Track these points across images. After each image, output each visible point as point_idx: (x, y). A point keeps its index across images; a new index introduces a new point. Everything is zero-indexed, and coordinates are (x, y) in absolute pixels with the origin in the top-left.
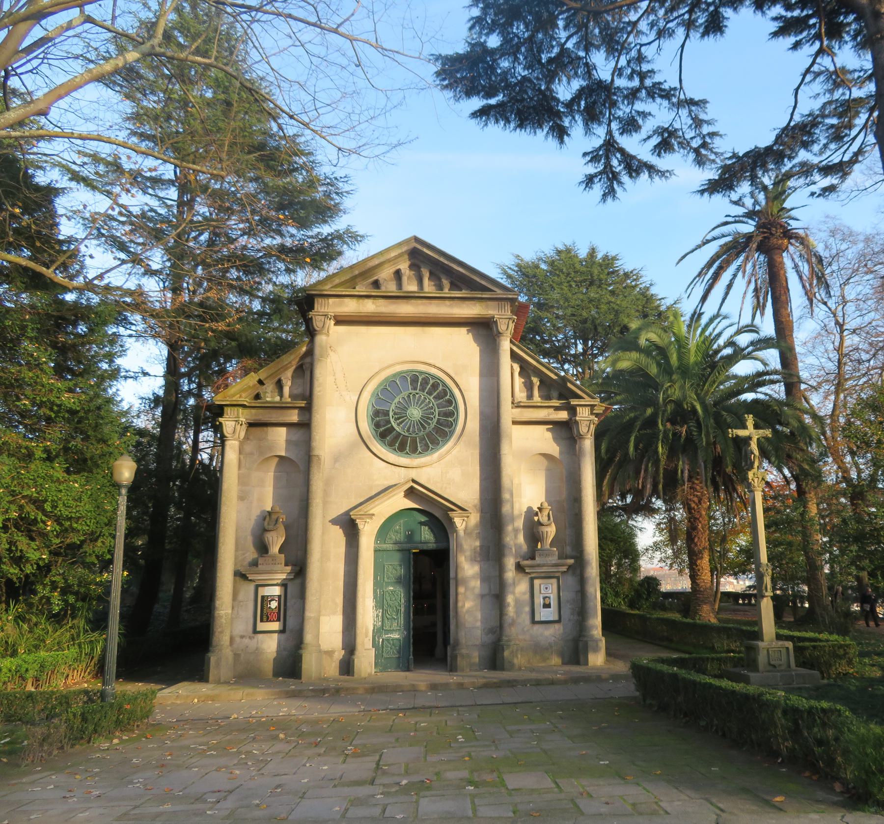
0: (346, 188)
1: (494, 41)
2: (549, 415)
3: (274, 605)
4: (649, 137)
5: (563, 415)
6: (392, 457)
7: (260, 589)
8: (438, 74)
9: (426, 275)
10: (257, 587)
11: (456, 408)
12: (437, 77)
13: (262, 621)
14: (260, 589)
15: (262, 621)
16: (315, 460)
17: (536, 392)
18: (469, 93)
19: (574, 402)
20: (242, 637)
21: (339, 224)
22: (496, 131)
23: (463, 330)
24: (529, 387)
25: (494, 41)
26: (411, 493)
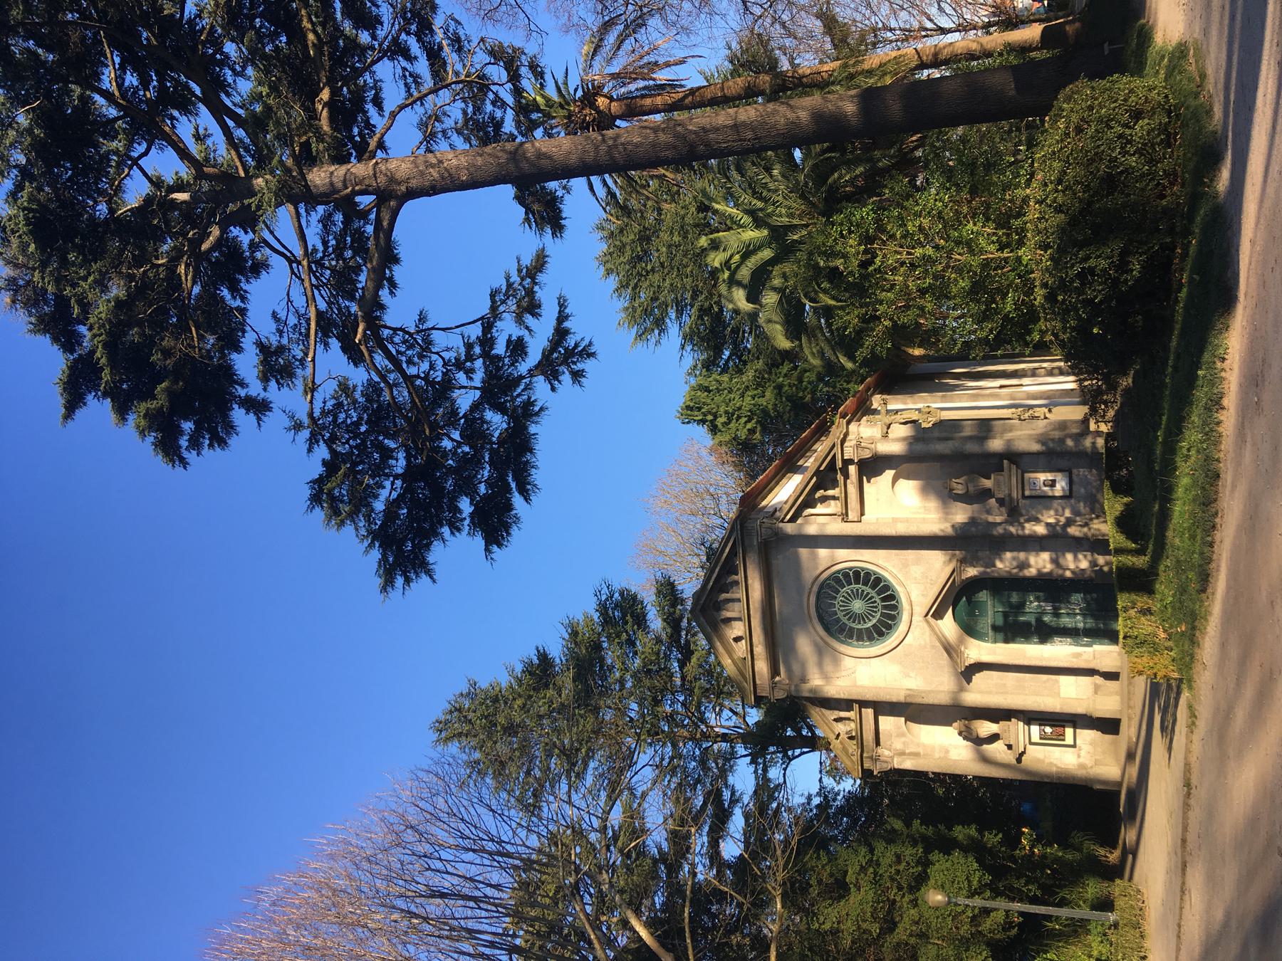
0: (605, 590)
1: (465, 506)
2: (852, 483)
3: (1048, 730)
4: (527, 328)
5: (852, 469)
6: (902, 627)
7: (1033, 740)
8: (500, 545)
9: (724, 596)
10: (1031, 743)
11: (850, 569)
12: (502, 545)
13: (1064, 740)
14: (1033, 740)
15: (1064, 740)
16: (909, 700)
17: (830, 492)
18: (509, 507)
19: (839, 464)
20: (1079, 756)
21: (648, 596)
22: (538, 476)
23: (774, 562)
24: (824, 499)
25: (465, 506)
26: (938, 615)
